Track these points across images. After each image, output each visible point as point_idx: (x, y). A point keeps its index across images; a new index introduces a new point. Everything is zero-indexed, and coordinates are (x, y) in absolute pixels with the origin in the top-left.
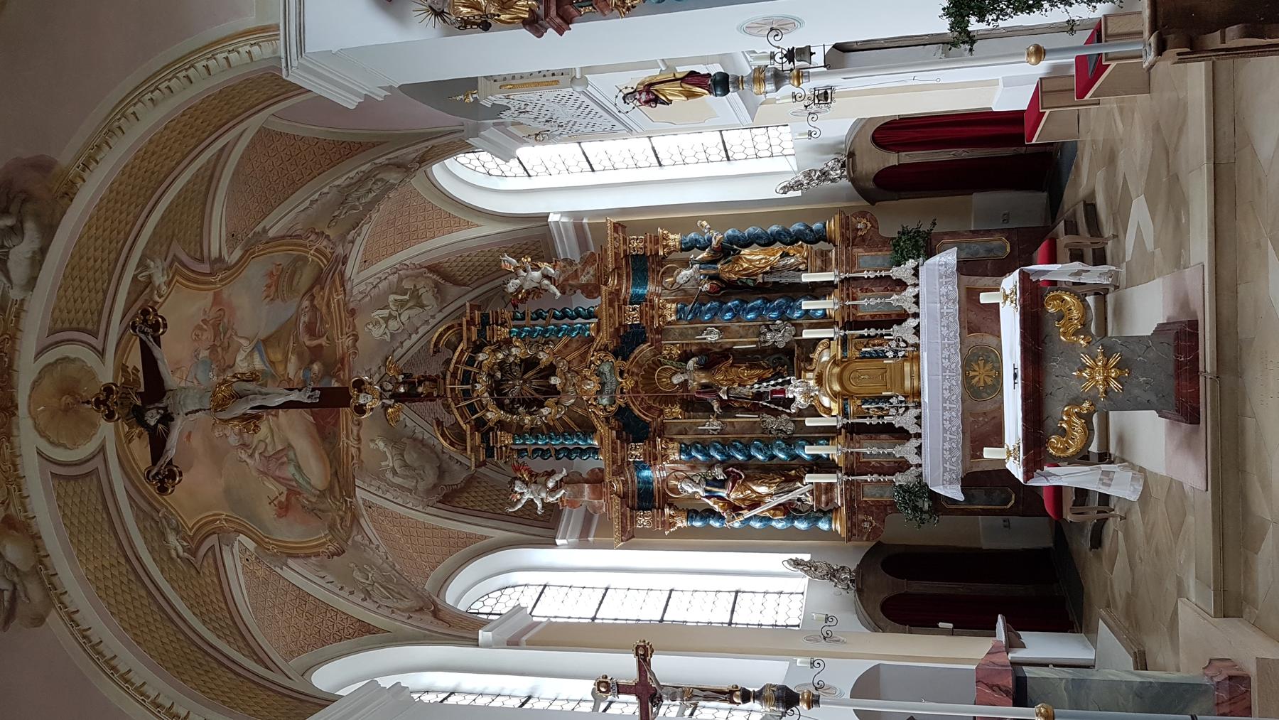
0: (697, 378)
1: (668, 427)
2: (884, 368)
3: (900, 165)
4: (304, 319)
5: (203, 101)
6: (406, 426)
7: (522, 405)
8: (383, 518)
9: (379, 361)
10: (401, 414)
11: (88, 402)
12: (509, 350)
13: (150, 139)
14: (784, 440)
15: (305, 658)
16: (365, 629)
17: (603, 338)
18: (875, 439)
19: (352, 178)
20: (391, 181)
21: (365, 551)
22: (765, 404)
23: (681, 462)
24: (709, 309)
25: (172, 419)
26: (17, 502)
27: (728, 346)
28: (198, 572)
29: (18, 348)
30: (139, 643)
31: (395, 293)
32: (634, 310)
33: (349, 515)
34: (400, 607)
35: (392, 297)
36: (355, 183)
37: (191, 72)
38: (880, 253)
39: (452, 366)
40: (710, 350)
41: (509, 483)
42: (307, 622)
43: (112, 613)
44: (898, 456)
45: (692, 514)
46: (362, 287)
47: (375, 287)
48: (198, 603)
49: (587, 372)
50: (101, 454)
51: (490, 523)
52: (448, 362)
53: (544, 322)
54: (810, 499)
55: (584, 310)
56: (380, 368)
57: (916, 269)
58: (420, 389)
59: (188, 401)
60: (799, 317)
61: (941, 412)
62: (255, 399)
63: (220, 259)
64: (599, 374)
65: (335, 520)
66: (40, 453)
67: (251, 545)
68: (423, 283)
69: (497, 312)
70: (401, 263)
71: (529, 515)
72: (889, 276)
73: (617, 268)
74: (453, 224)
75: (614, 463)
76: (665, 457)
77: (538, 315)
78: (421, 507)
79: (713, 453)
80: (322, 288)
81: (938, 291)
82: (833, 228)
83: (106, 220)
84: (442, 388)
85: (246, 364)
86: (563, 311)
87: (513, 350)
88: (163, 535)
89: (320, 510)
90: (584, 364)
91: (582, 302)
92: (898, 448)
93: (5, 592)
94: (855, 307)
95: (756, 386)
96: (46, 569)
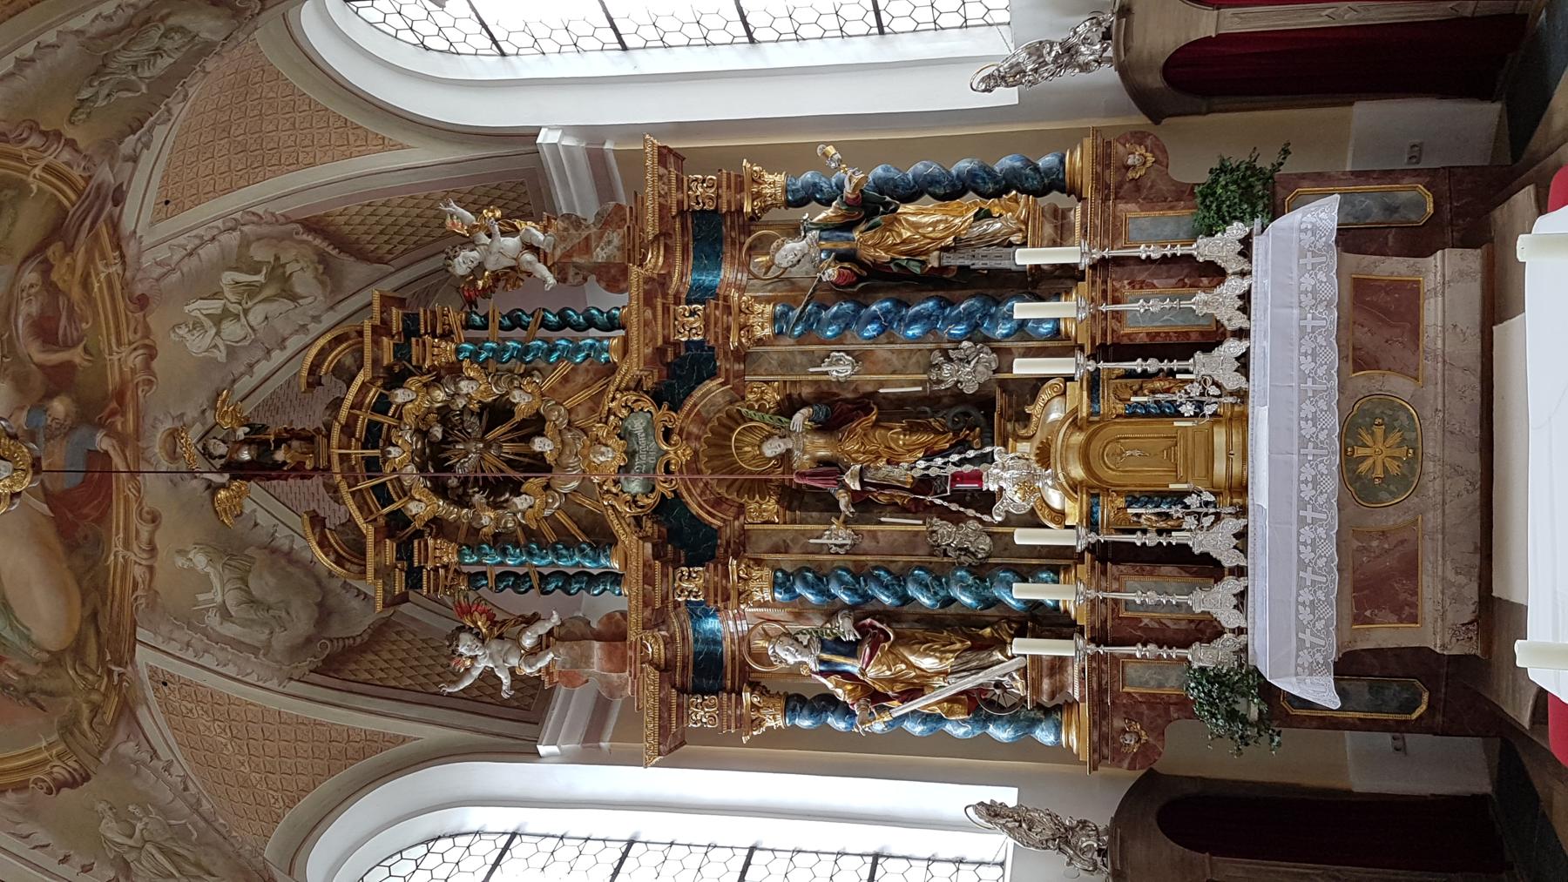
0: (809, 448)
1: (753, 539)
2: (1174, 439)
3: (1219, 36)
4: (28, 309)
6: (256, 524)
7: (483, 489)
8: (189, 706)
9: (202, 399)
14: (971, 569)
17: (632, 368)
18: (1151, 574)
19: (109, 18)
20: (205, 35)
21: (137, 774)
22: (938, 502)
23: (774, 604)
24: (835, 317)
27: (869, 389)
31: (236, 269)
32: (693, 313)
33: (114, 700)
35: (228, 277)
36: (119, 31)
38: (1171, 213)
39: (344, 413)
40: (835, 394)
44: (1198, 611)
45: (794, 702)
46: (163, 253)
47: (190, 254)
49: (601, 431)
51: (415, 711)
52: (336, 404)
53: (524, 333)
54: (1020, 684)
55: (601, 313)
56: (203, 412)
57: (1246, 242)
58: (280, 456)
60: (1007, 336)
61: (1295, 527)
64: (625, 435)
69: (433, 312)
70: (244, 210)
71: (490, 696)
72: (1191, 256)
73: (664, 234)
74: (352, 140)
75: (646, 605)
76: (745, 596)
77: (515, 321)
78: (275, 681)
79: (835, 589)
80: (69, 249)
81: (1295, 282)
82: (1078, 164)
84: (323, 455)
86: (562, 314)
90: (596, 417)
91: (604, 301)
92: (1199, 595)
94: (1118, 316)
95: (922, 464)
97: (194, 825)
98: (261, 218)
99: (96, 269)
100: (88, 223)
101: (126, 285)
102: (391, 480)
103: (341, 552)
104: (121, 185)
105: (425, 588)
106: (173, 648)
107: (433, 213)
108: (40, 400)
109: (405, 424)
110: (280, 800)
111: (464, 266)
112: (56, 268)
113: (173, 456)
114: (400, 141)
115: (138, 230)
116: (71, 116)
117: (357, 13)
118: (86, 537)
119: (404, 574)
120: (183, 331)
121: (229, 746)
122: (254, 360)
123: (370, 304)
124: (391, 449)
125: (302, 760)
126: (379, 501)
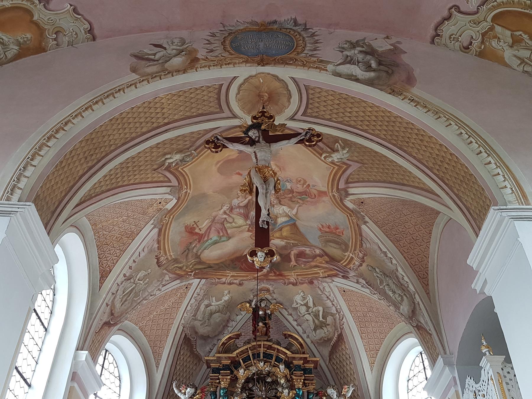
4: (308, 250)
5: (462, 165)
6: (237, 315)
8: (178, 295)
9: (280, 299)
10: (245, 312)
11: (263, 108)
12: (287, 388)
13: (432, 137)
15: (90, 234)
16: (104, 275)
19: (403, 279)
20: (402, 307)
25: (251, 146)
26: (207, 64)
28: (155, 170)
29: (298, 67)
30: (111, 120)
31: (323, 312)
34: (116, 299)
35: (321, 309)
36: (400, 282)
37: (484, 155)
39: (276, 346)
41: (193, 384)
42: (115, 237)
43: (133, 108)
46: (327, 289)
47: (328, 297)
48: (135, 166)
50: (232, 116)
52: (279, 344)
56: (275, 299)
58: (261, 324)
59: (263, 153)
62: (263, 189)
63: (347, 194)
65: (180, 263)
66: (235, 78)
67: (169, 206)
68: (331, 330)
69: (313, 380)
70: (344, 315)
74: (372, 353)
78: (184, 322)
80: (327, 262)
83: (376, 117)
85: (281, 212)
87: (287, 390)
88: (180, 151)
89: (188, 254)
93: (154, 56)
96: (164, 75)
97: (139, 299)
98: (342, 320)
99: (321, 269)
100: (336, 268)
101: (317, 278)
102: (252, 362)
103: (227, 345)
104: (349, 278)
105: (212, 375)
106: (198, 290)
107: (349, 380)
108: (279, 253)
109: (272, 368)
110: (143, 325)
111: (330, 392)
112: (321, 258)
113: (261, 290)
114: (373, 369)
115: (334, 282)
116: (370, 266)
117: (417, 356)
118: (235, 265)
119: (218, 367)
120: (302, 294)
121: (163, 308)
122: (293, 316)
123: (315, 357)
124: (263, 363)
125: (155, 332)
126: (244, 358)
